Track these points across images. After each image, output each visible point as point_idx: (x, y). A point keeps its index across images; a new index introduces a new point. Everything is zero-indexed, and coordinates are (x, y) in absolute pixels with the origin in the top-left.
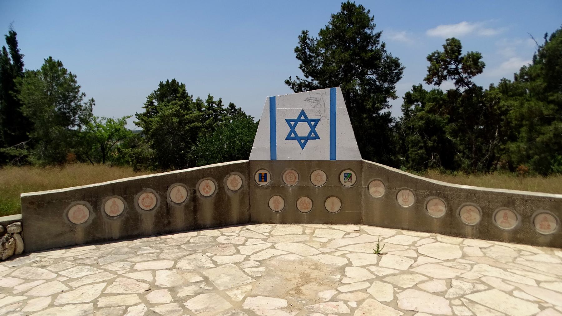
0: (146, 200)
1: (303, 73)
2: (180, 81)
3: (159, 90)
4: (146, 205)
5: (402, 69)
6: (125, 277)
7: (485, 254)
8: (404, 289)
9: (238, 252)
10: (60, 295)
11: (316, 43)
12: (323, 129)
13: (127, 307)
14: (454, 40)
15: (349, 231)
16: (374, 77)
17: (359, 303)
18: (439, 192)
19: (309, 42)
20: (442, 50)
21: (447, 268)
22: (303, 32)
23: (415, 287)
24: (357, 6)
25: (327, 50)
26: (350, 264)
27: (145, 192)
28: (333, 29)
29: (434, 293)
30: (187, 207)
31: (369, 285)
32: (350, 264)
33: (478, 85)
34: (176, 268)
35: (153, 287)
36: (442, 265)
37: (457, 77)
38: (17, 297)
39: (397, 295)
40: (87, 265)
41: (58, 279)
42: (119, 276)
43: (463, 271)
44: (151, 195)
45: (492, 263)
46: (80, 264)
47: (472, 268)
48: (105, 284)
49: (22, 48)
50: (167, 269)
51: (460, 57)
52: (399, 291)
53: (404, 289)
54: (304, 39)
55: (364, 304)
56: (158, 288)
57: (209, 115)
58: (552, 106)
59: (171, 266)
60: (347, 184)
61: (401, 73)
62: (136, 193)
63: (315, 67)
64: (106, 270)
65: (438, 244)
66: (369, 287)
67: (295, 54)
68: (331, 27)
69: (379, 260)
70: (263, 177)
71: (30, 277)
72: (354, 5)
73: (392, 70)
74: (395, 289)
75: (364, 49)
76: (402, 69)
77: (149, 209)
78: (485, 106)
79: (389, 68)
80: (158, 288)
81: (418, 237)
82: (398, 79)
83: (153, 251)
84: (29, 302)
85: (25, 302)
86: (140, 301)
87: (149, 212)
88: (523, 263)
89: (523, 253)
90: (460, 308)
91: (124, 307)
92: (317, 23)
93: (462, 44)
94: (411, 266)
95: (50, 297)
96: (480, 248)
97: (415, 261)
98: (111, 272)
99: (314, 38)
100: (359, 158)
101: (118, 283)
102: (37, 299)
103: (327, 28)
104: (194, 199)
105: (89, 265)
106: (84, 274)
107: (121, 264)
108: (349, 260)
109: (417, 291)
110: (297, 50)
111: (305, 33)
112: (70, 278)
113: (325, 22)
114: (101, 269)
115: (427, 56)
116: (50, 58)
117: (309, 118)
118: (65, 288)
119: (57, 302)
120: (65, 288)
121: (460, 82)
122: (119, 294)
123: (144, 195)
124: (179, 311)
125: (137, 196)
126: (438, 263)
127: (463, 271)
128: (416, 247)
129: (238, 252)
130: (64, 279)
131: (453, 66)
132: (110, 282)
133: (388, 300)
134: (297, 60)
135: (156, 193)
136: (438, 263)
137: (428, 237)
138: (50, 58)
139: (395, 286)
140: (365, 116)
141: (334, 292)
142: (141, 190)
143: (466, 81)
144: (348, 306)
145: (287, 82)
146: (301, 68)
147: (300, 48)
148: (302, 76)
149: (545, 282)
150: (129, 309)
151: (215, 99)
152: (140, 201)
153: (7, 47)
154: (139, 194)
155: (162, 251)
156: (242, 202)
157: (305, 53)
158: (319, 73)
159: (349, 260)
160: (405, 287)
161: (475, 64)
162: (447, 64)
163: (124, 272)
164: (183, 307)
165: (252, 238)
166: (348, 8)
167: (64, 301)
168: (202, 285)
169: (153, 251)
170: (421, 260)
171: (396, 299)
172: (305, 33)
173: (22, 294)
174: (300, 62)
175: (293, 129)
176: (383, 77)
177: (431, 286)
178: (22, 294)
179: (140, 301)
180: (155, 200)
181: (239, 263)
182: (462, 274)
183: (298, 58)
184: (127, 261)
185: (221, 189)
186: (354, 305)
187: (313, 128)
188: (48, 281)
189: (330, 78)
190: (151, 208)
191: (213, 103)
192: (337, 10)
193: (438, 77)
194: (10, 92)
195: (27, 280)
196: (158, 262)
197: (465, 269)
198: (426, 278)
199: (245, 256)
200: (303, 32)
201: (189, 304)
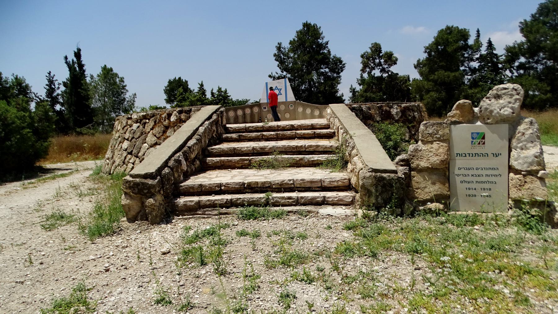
1: (280, 70)
2: (184, 79)
3: (168, 86)
5: (344, 64)
11: (287, 50)
12: (283, 92)
14: (376, 44)
16: (327, 70)
19: (282, 50)
20: (369, 51)
22: (279, 44)
24: (312, 25)
25: (295, 54)
28: (297, 41)
33: (395, 72)
37: (381, 67)
49: (84, 59)
51: (381, 54)
54: (279, 48)
57: (219, 100)
58: (431, 83)
60: (291, 108)
61: (344, 67)
63: (288, 65)
67: (274, 58)
68: (296, 39)
70: (265, 108)
72: (310, 24)
73: (337, 66)
75: (318, 53)
76: (344, 64)
79: (336, 64)
82: (342, 71)
92: (287, 36)
93: (382, 47)
99: (286, 47)
100: (295, 100)
103: (294, 40)
104: (244, 114)
110: (275, 55)
111: (280, 44)
113: (293, 36)
115: (360, 55)
116: (105, 66)
121: (383, 70)
131: (377, 61)
134: (276, 62)
138: (105, 66)
140: (320, 95)
143: (387, 70)
145: (270, 76)
146: (278, 66)
147: (277, 54)
148: (279, 71)
151: (223, 90)
153: (75, 60)
156: (258, 116)
157: (281, 57)
158: (291, 69)
161: (390, 59)
162: (374, 59)
166: (307, 25)
172: (280, 44)
174: (278, 63)
176: (332, 70)
183: (276, 60)
185: (252, 111)
187: (280, 91)
189: (298, 72)
191: (222, 92)
192: (300, 27)
193: (369, 68)
194: (79, 90)
200: (279, 44)
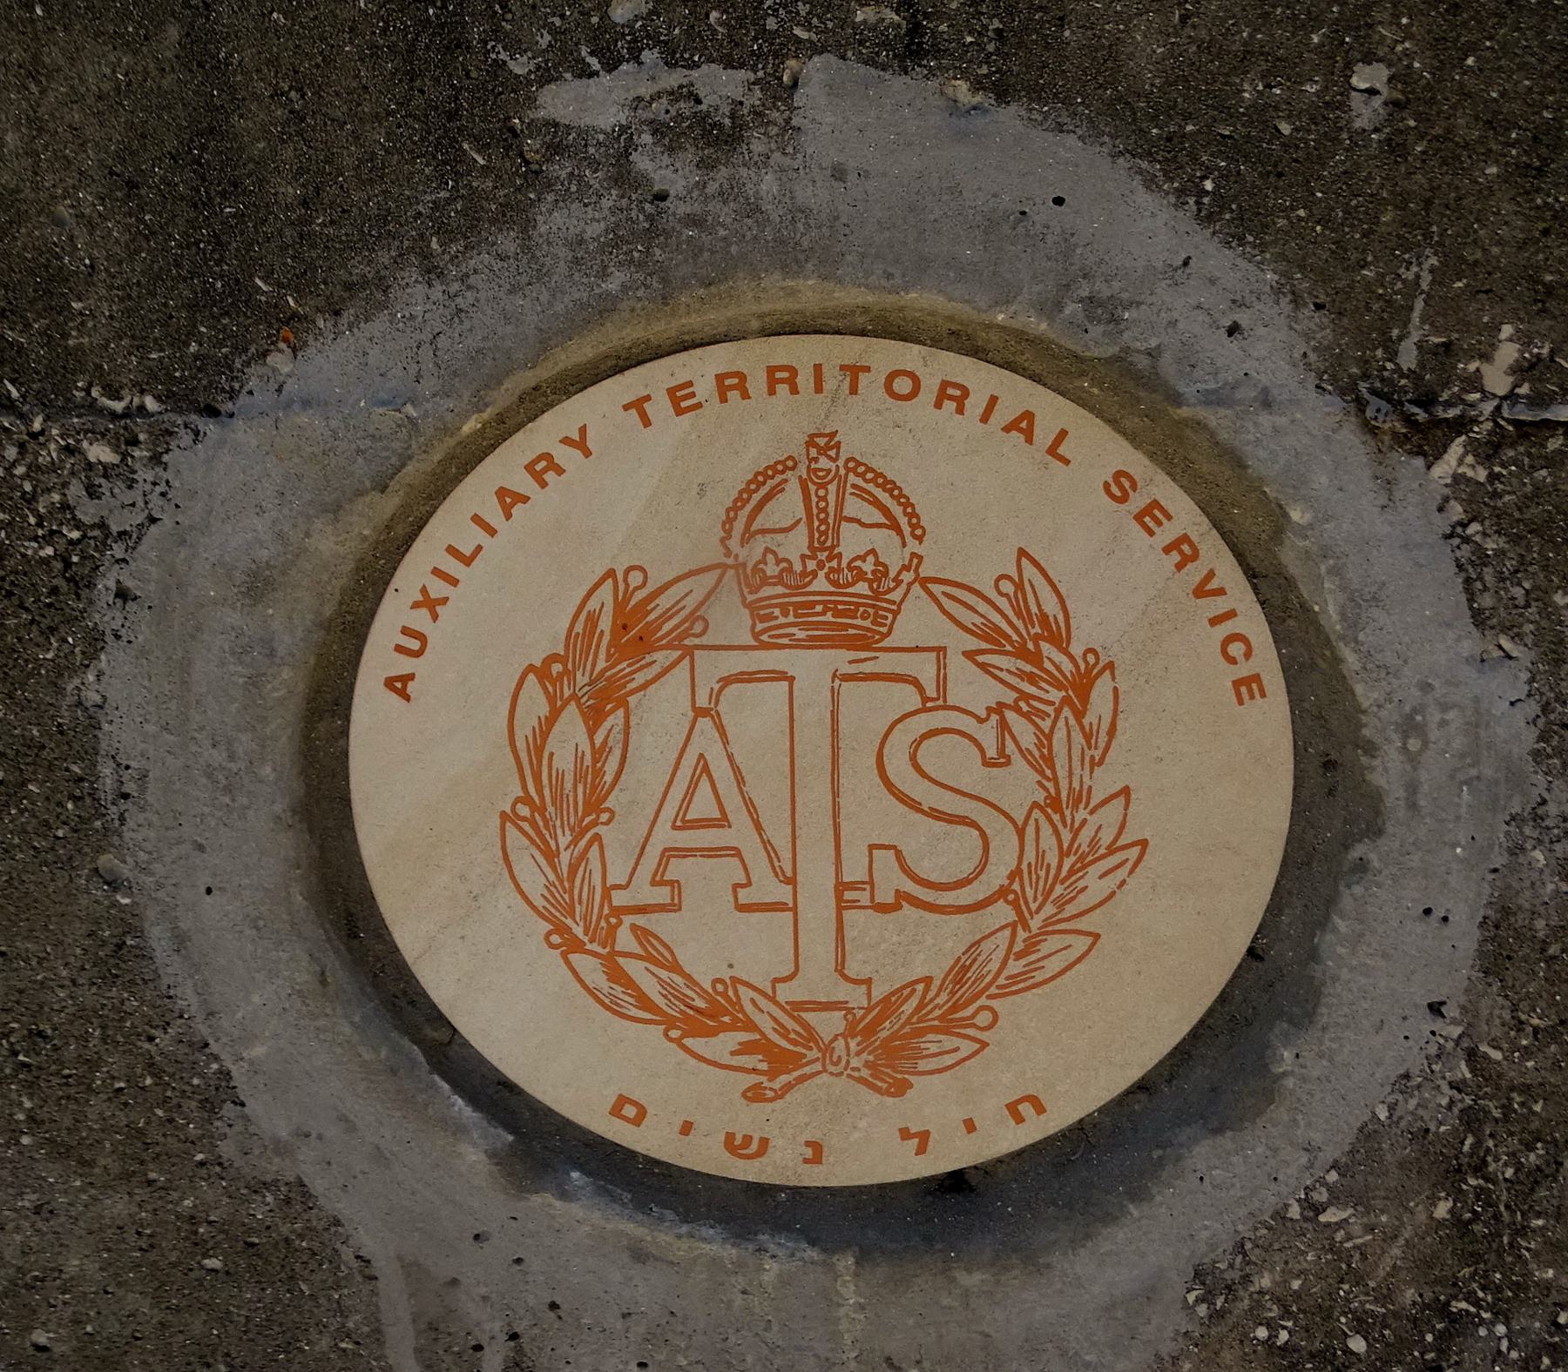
0: (755, 720)
4: (715, 943)
27: (669, 281)
44: (1005, 486)
62: (218, 308)
77: (871, 1142)
78: (192, 141)
87: (848, 1295)
117: (433, 596)
123: (619, 481)
125: (230, 497)
135: (1314, 454)
142: (463, 156)
152: (425, 771)
154: (335, 378)
180: (1206, 795)
190: (965, 1115)
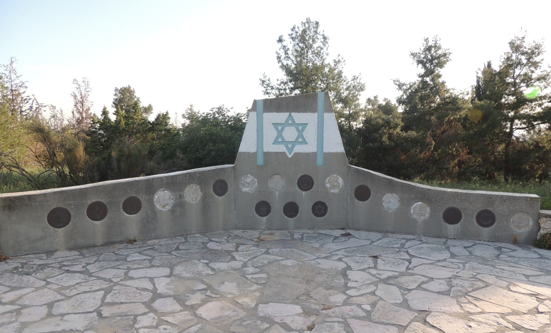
6: (121, 285)
7: (470, 252)
8: (410, 290)
9: (233, 259)
10: (56, 304)
13: (136, 316)
15: (337, 235)
17: (373, 305)
18: (424, 196)
21: (441, 268)
23: (419, 287)
26: (349, 268)
29: (439, 293)
30: (172, 211)
31: (375, 288)
32: (349, 268)
34: (174, 276)
35: (156, 296)
36: (437, 266)
38: (7, 306)
39: (406, 296)
40: (75, 272)
41: (48, 286)
42: (116, 284)
43: (458, 271)
45: (481, 262)
46: (68, 271)
47: (464, 266)
48: (103, 292)
50: (163, 277)
52: (405, 292)
53: (410, 290)
55: (378, 306)
56: (161, 296)
59: (168, 274)
64: (99, 278)
65: (424, 245)
66: (376, 290)
69: (376, 263)
71: (15, 285)
74: (401, 290)
80: (161, 296)
81: (403, 239)
83: (144, 257)
84: (22, 311)
85: (18, 312)
86: (147, 310)
88: (507, 259)
89: (503, 250)
90: (468, 305)
91: (132, 317)
94: (408, 268)
95: (46, 306)
96: (465, 247)
97: (410, 263)
98: (104, 279)
101: (116, 292)
102: (31, 309)
105: (78, 272)
106: (75, 282)
107: (115, 271)
108: (346, 263)
109: (423, 292)
112: (62, 286)
114: (93, 276)
118: (59, 297)
119: (55, 311)
120: (59, 297)
122: (122, 303)
124: (192, 320)
126: (432, 264)
127: (458, 271)
128: (406, 249)
129: (233, 259)
130: (55, 287)
132: (107, 292)
133: (399, 302)
136: (432, 264)
137: (414, 239)
139: (400, 288)
141: (345, 297)
144: (363, 309)
149: (532, 276)
150: (138, 318)
155: (153, 258)
159: (346, 263)
160: (409, 288)
163: (119, 279)
164: (195, 315)
165: (243, 244)
167: (62, 311)
168: (208, 293)
169: (144, 257)
170: (415, 261)
171: (406, 300)
173: (12, 303)
175: (280, 133)
177: (433, 286)
178: (12, 303)
179: (147, 310)
181: (239, 269)
182: (457, 273)
184: (118, 268)
186: (368, 308)
188: (37, 289)
195: (13, 289)
196: (152, 269)
197: (459, 268)
198: (425, 279)
199: (242, 263)
201: (202, 312)
